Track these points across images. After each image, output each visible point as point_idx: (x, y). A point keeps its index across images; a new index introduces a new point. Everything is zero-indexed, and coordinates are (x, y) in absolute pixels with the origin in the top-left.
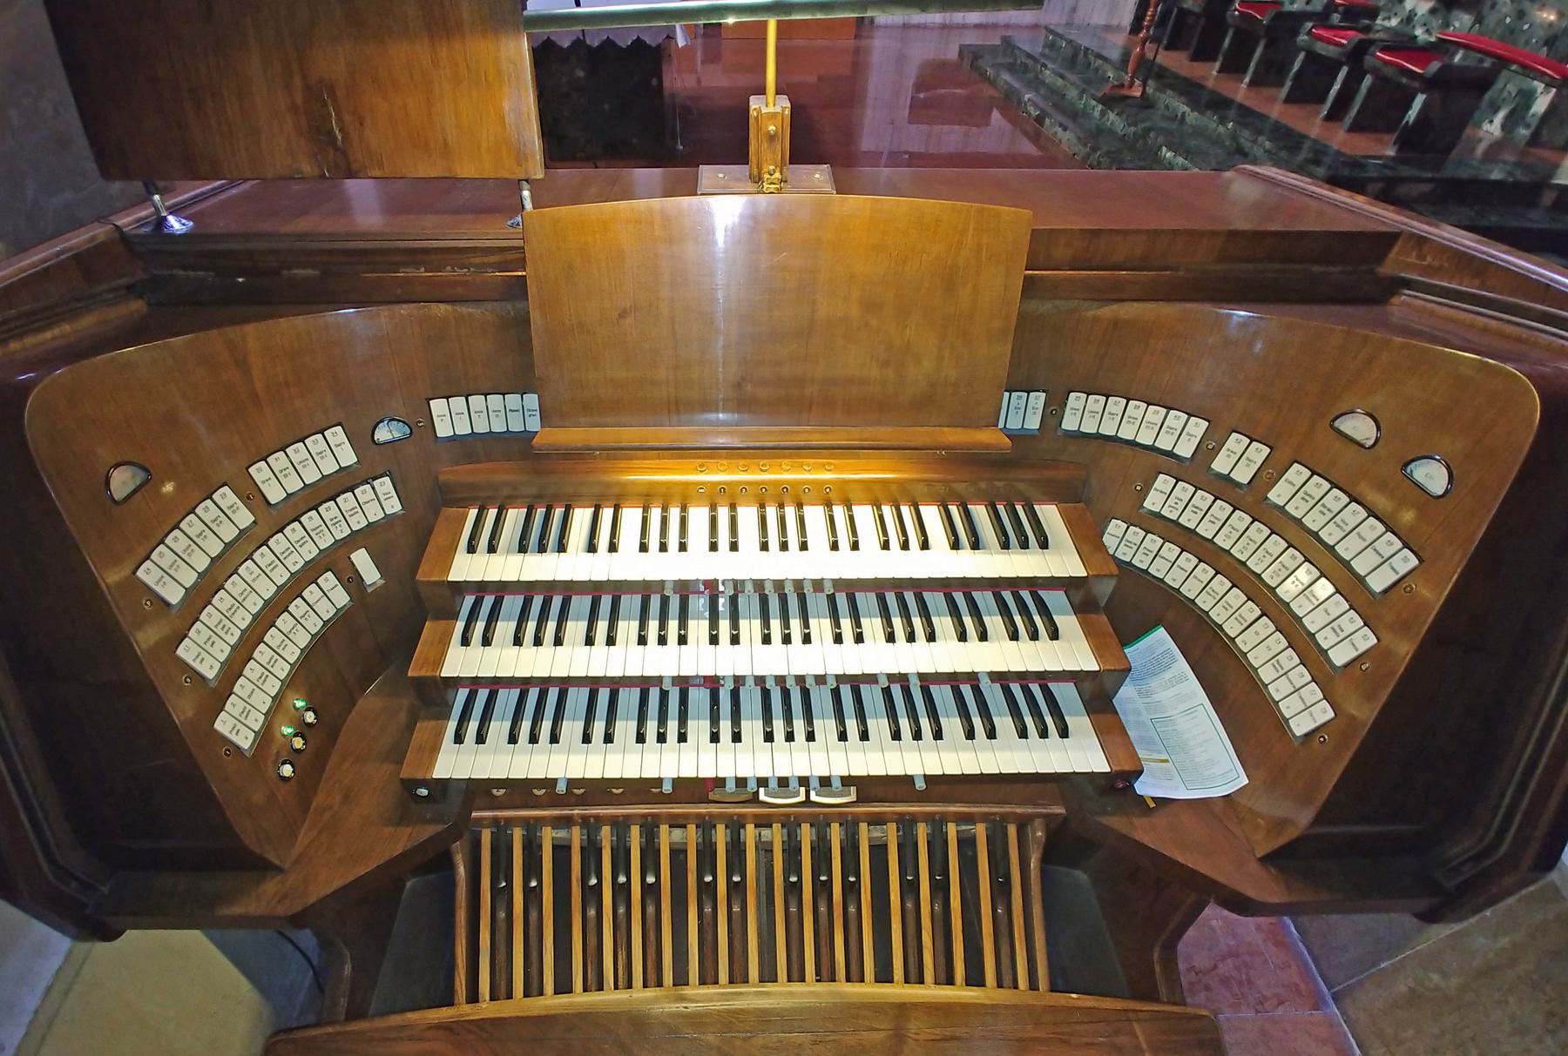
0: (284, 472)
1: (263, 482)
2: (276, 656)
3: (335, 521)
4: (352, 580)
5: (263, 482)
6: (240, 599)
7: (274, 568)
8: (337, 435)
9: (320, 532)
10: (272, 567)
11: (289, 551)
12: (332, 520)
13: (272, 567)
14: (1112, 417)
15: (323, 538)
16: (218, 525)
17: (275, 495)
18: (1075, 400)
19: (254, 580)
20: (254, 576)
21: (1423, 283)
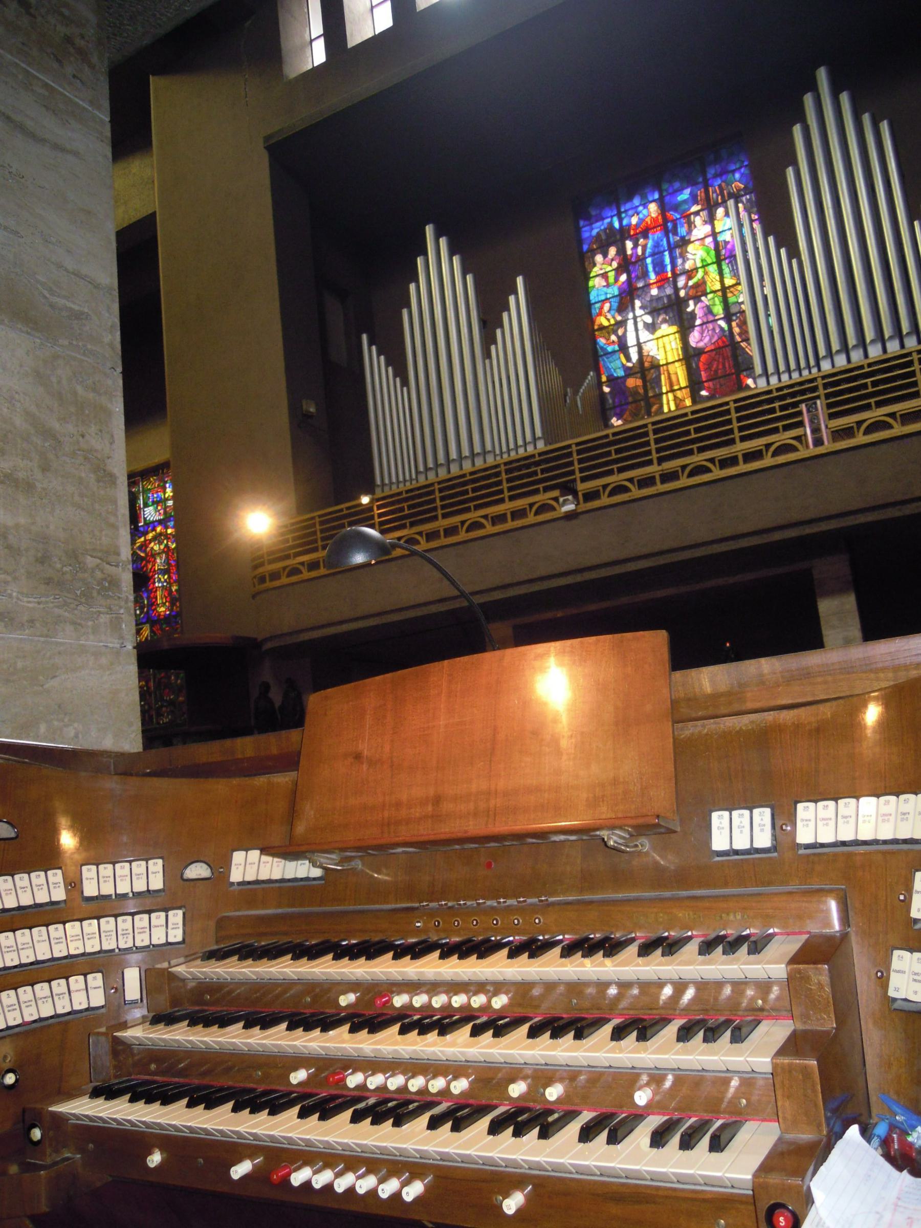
0: (105, 879)
1: (87, 879)
2: (17, 1006)
3: (125, 932)
4: (115, 989)
5: (87, 879)
6: (20, 947)
7: (59, 943)
8: (157, 865)
9: (109, 935)
10: (58, 941)
11: (78, 938)
12: (123, 930)
13: (58, 941)
14: (845, 820)
15: (109, 941)
16: (38, 890)
17: (90, 890)
18: (805, 811)
19: (39, 941)
20: (41, 939)
21: (684, 427)
